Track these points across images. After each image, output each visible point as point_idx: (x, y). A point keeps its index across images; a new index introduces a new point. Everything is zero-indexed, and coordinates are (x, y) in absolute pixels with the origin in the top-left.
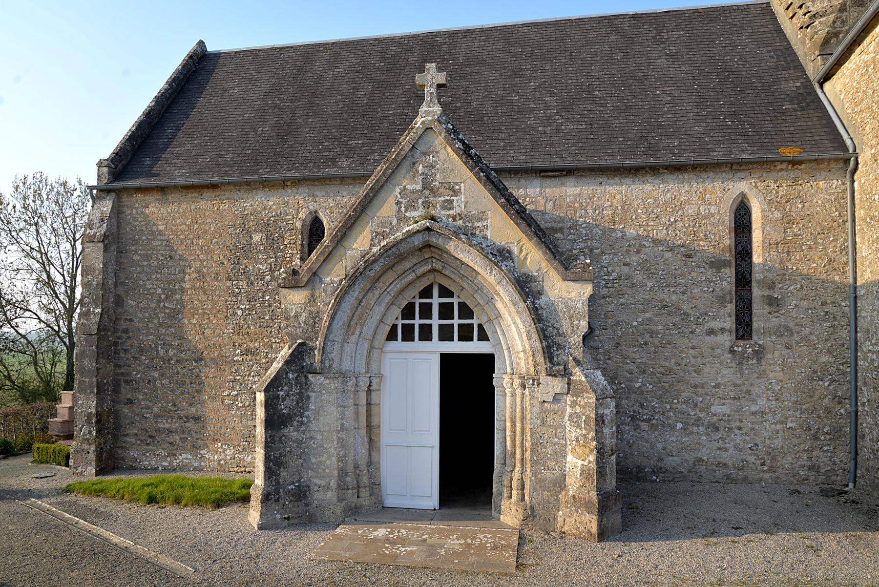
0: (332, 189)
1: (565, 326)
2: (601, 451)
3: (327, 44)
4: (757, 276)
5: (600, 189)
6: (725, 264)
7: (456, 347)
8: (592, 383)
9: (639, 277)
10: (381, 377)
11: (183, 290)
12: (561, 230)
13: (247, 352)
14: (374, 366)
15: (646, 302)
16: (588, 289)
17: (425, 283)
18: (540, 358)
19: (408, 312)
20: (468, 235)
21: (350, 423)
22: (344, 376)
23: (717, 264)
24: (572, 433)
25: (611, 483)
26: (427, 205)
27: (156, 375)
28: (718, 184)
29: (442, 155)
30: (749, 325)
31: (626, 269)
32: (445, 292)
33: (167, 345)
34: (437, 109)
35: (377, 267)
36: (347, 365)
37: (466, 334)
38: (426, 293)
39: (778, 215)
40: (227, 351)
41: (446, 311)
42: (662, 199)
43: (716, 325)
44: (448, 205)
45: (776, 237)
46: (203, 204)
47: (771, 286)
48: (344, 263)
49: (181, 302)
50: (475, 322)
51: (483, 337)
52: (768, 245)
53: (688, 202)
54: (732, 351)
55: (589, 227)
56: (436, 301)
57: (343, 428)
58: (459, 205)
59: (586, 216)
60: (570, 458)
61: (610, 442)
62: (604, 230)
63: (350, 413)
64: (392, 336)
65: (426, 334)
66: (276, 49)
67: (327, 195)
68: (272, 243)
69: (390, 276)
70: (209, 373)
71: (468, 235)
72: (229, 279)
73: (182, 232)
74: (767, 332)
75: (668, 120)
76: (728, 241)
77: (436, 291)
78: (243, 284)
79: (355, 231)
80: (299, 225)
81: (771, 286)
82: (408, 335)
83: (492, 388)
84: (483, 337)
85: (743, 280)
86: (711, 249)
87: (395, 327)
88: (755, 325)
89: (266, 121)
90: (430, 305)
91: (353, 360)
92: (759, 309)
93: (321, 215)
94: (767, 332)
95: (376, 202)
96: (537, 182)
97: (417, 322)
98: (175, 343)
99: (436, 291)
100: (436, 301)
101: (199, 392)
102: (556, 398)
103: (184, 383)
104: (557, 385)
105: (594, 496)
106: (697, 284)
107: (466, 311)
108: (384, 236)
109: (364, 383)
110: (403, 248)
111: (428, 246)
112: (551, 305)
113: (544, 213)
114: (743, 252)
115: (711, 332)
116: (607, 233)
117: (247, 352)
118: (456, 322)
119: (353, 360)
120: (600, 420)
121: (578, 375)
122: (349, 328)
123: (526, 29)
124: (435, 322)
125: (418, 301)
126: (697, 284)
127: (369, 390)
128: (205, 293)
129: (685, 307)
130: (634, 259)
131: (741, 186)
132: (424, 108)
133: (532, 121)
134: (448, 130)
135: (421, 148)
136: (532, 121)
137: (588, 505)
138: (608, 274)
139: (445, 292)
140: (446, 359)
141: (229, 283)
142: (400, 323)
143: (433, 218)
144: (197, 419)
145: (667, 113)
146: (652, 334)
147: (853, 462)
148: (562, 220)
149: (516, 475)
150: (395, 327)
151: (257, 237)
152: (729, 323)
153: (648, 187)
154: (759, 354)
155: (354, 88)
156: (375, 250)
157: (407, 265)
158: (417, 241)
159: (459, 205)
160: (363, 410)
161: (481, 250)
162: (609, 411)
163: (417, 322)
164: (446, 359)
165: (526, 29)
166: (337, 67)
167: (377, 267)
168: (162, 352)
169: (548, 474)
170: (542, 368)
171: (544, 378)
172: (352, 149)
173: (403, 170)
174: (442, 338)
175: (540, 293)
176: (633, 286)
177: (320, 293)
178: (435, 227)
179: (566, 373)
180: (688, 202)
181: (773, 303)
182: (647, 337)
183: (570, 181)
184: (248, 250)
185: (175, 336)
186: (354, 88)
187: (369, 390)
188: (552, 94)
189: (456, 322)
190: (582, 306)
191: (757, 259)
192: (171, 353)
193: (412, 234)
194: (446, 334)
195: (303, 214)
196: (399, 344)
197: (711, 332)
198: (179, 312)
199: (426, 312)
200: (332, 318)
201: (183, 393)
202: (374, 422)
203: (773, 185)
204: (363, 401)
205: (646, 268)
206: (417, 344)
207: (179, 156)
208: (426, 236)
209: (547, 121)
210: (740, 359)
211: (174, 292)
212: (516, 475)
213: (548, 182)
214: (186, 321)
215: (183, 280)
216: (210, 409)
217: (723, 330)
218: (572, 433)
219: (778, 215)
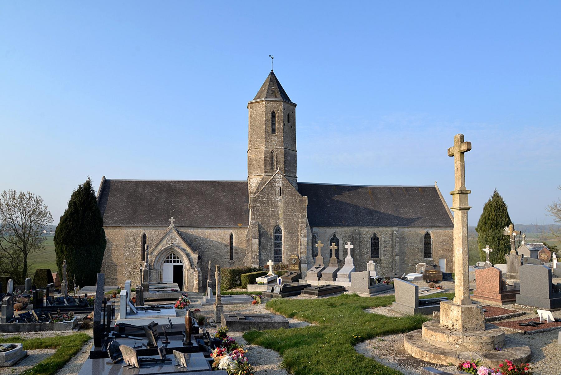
0: (148, 228)
1: (194, 261)
2: (199, 281)
3: (142, 181)
4: (234, 248)
5: (205, 231)
6: (228, 246)
7: (176, 264)
8: (198, 270)
9: (212, 248)
10: (163, 270)
11: (112, 250)
12: (197, 238)
13: (129, 263)
14: (161, 268)
15: (213, 253)
16: (198, 255)
17: (171, 253)
18: (190, 266)
19: (168, 258)
20: (178, 246)
21: (157, 278)
22: (157, 270)
23: (227, 246)
24: (195, 278)
25: (201, 286)
26: (171, 241)
27: (105, 269)
28: (227, 230)
29: (174, 233)
30: (233, 257)
31: (210, 246)
32: (174, 255)
33: (108, 262)
34: (173, 225)
35: (163, 252)
36: (157, 268)
37: (178, 262)
38: (171, 255)
39: (237, 237)
40: (124, 264)
41: (174, 258)
42: (217, 233)
43: (226, 257)
44: (175, 241)
45: (237, 241)
46: (117, 230)
47: (236, 250)
48: (157, 251)
49: (111, 252)
50: (179, 260)
51: (181, 262)
52: (236, 243)
53: (222, 234)
54: (229, 262)
55: (203, 238)
56: (173, 256)
57: (156, 279)
58: (177, 241)
59: (202, 236)
60: (195, 282)
61: (201, 279)
62: (206, 239)
63: (157, 276)
64: (165, 262)
65: (171, 262)
66: (127, 181)
67: (147, 229)
68: (134, 239)
69: (165, 253)
70: (118, 269)
71: (178, 246)
72: (124, 247)
73: (112, 236)
74: (235, 259)
75: (220, 215)
76: (229, 241)
77: (173, 254)
78: (127, 249)
79: (159, 245)
80: (141, 236)
81: (236, 250)
82: (168, 262)
83: (182, 271)
84: (181, 262)
85: (232, 248)
86: (225, 243)
87: (165, 261)
88: (234, 257)
89: (129, 207)
90: (174, 259)
91: (158, 267)
92: (234, 254)
93: (146, 234)
94: (235, 259)
95: (163, 240)
96: (193, 229)
97: (169, 260)
98: (110, 262)
99: (173, 254)
100: (173, 256)
101: (116, 273)
102: (192, 273)
103: (112, 271)
104: (193, 270)
105: (198, 287)
106: (223, 249)
107: (178, 258)
108: (164, 246)
109: (160, 271)
110: (167, 248)
111: (172, 248)
112: (192, 258)
113: (194, 235)
114: (232, 243)
115: (225, 259)
116: (206, 239)
117: (129, 263)
118: (176, 260)
119: (158, 267)
120: (199, 276)
121: (196, 269)
122: (157, 262)
123: (193, 183)
124: (173, 260)
125: (169, 256)
126: (223, 249)
127: (161, 272)
128: (118, 250)
129: (221, 254)
130: (211, 244)
131: (231, 231)
132: (171, 225)
133: (192, 213)
134: (175, 229)
135: (170, 232)
136: (192, 213)
137: (197, 289)
138: (206, 247)
139: (174, 255)
140: (174, 266)
141: (124, 248)
142: (166, 260)
143: (173, 244)
144: (116, 279)
145: (220, 213)
146: (215, 259)
147: (28, 264)
148: (198, 236)
149: (186, 285)
150: (165, 261)
151: (131, 238)
152: (229, 257)
153: (214, 230)
154: (234, 263)
155: (151, 198)
156: (163, 249)
157: (168, 251)
158: (170, 247)
159: (177, 241)
160: (160, 276)
161: (181, 249)
162: (201, 274)
163: (169, 260)
164: (174, 266)
165: (193, 183)
166: (146, 191)
167: (163, 252)
168: (107, 264)
169: (191, 285)
170: (190, 268)
171: (190, 269)
172: (152, 218)
173: (167, 235)
174: (174, 262)
175: (190, 256)
176: (211, 250)
177: (153, 256)
178: (173, 245)
179: (194, 269)
180: (222, 234)
181: (236, 253)
182: (214, 260)
183: (199, 229)
184: (128, 241)
185: (110, 260)
186: (151, 198)
187: (161, 272)
188: (197, 205)
189: (176, 260)
190: (197, 258)
191: (234, 245)
192: (109, 264)
193: (169, 246)
194: (174, 262)
195: (142, 233)
196: (166, 264)
197: (225, 259)
198: (111, 255)
199: (171, 258)
200: (155, 260)
201: (112, 273)
202: (162, 277)
203: (237, 231)
204: (160, 274)
205: (213, 246)
206: (169, 263)
207: (108, 217)
208: (171, 247)
209: (195, 213)
210: (230, 264)
211: (110, 250)
212: (186, 285)
213: (195, 229)
214: (113, 257)
215: (112, 247)
216: (119, 277)
217: (227, 258)
218: (195, 278)
219: (237, 237)
